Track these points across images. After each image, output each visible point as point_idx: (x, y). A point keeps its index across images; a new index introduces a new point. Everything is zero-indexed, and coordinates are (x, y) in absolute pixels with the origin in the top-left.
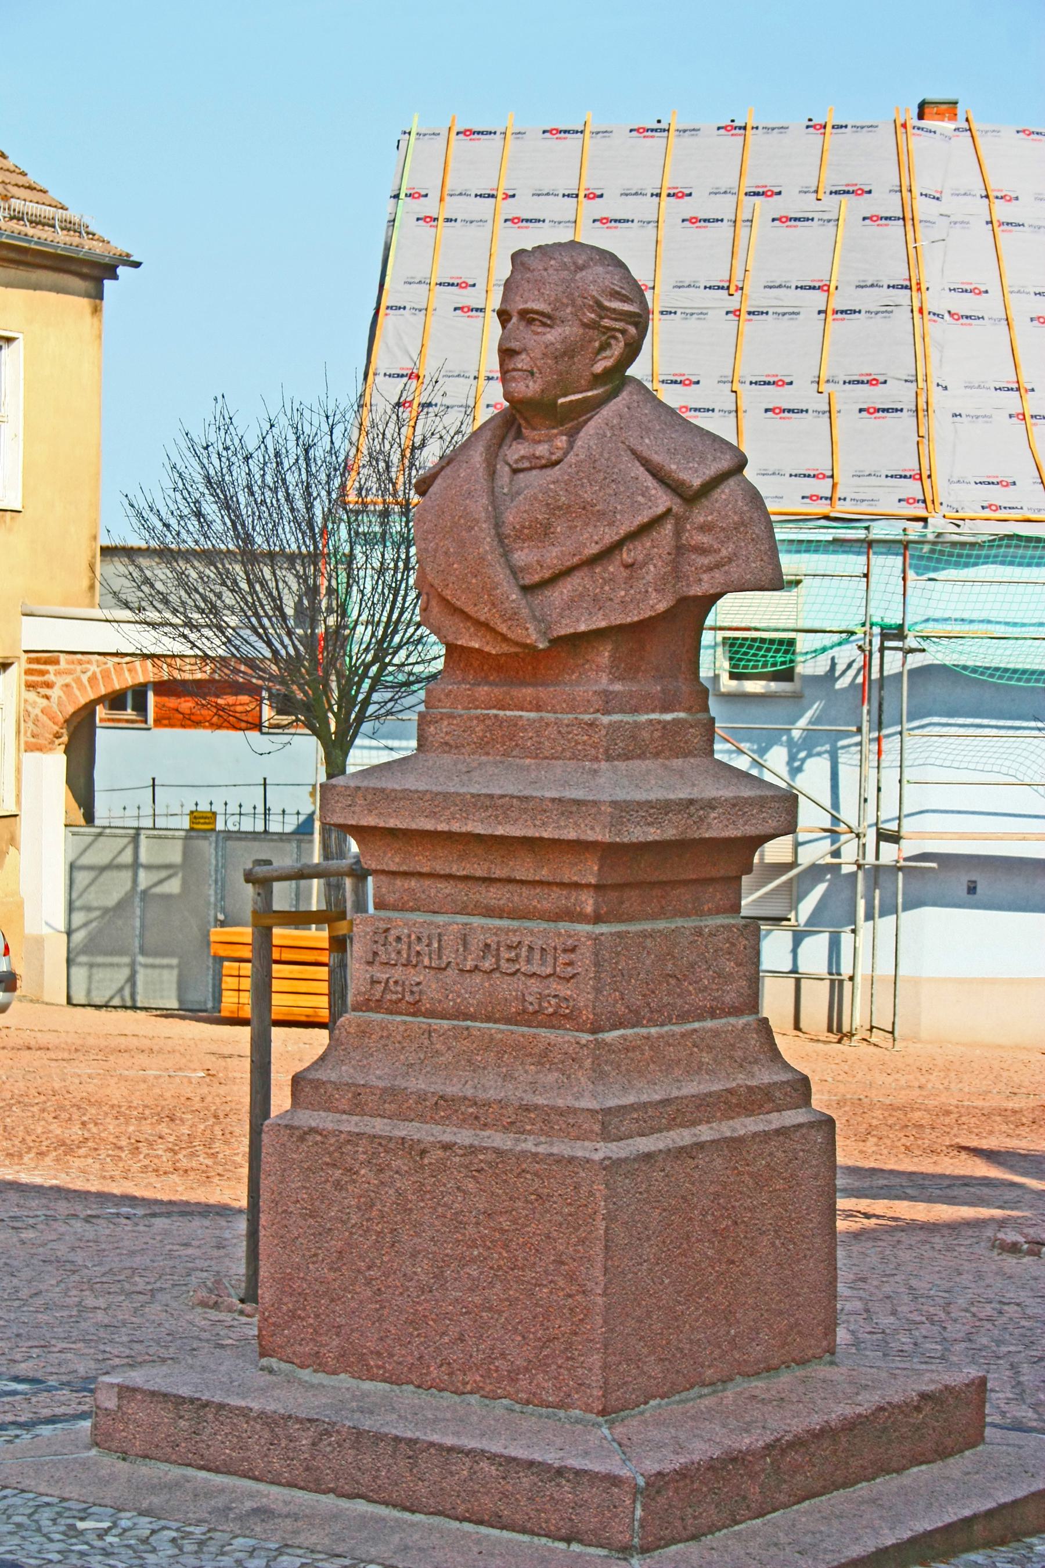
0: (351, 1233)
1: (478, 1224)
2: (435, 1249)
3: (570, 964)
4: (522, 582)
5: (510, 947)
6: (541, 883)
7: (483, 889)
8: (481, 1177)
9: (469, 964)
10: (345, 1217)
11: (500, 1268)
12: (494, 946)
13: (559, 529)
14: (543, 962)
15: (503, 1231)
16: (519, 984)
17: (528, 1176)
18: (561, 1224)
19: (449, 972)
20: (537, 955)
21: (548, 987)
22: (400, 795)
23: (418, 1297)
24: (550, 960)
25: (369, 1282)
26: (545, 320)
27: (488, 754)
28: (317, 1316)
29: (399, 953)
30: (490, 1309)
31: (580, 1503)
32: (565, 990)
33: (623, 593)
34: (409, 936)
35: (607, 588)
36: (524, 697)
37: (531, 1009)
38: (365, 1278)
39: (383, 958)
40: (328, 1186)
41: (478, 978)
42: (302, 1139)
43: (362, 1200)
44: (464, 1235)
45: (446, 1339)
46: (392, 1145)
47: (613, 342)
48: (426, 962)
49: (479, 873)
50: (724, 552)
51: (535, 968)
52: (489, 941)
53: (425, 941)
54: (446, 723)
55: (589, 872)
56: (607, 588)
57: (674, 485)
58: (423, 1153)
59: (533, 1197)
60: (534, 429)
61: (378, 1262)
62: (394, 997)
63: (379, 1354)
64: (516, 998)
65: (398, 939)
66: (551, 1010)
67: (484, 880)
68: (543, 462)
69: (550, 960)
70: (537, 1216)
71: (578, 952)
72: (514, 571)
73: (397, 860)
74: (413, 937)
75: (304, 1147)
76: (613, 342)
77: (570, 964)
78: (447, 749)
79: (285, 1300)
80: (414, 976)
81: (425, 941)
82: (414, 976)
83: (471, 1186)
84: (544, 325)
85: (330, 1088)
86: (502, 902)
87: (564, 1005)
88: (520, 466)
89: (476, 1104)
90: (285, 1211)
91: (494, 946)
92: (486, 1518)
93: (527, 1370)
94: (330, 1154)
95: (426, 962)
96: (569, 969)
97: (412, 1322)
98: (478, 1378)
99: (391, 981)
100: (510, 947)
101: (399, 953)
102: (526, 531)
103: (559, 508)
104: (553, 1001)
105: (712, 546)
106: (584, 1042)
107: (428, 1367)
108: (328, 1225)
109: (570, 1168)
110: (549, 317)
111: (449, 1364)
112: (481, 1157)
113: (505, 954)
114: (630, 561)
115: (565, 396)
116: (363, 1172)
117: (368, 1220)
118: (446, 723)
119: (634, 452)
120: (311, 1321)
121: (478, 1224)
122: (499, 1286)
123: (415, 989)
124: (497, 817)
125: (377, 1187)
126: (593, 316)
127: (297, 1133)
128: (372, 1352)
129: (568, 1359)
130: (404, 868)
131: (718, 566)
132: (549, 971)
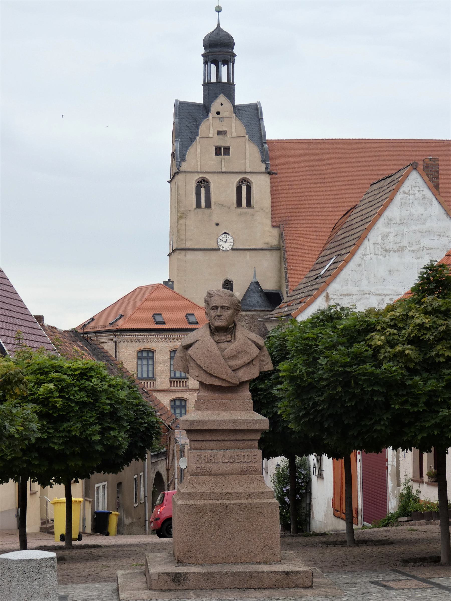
3: (255, 458)
5: (238, 456)
6: (243, 440)
7: (226, 443)
8: (244, 510)
9: (226, 461)
12: (233, 456)
14: (248, 458)
16: (241, 465)
25: (211, 540)
28: (196, 550)
29: (205, 460)
30: (248, 541)
32: (254, 465)
36: (319, 400)
39: (200, 461)
40: (198, 518)
41: (228, 464)
46: (218, 505)
48: (213, 461)
49: (226, 439)
58: (227, 506)
63: (215, 557)
69: (250, 457)
72: (230, 367)
75: (190, 509)
77: (255, 458)
81: (213, 456)
82: (209, 465)
83: (242, 512)
84: (227, 309)
85: (194, 494)
88: (219, 341)
91: (233, 456)
93: (259, 554)
94: (199, 510)
100: (238, 456)
101: (205, 460)
104: (251, 468)
119: (249, 339)
122: (250, 535)
130: (203, 439)
131: (267, 364)
132: (250, 460)
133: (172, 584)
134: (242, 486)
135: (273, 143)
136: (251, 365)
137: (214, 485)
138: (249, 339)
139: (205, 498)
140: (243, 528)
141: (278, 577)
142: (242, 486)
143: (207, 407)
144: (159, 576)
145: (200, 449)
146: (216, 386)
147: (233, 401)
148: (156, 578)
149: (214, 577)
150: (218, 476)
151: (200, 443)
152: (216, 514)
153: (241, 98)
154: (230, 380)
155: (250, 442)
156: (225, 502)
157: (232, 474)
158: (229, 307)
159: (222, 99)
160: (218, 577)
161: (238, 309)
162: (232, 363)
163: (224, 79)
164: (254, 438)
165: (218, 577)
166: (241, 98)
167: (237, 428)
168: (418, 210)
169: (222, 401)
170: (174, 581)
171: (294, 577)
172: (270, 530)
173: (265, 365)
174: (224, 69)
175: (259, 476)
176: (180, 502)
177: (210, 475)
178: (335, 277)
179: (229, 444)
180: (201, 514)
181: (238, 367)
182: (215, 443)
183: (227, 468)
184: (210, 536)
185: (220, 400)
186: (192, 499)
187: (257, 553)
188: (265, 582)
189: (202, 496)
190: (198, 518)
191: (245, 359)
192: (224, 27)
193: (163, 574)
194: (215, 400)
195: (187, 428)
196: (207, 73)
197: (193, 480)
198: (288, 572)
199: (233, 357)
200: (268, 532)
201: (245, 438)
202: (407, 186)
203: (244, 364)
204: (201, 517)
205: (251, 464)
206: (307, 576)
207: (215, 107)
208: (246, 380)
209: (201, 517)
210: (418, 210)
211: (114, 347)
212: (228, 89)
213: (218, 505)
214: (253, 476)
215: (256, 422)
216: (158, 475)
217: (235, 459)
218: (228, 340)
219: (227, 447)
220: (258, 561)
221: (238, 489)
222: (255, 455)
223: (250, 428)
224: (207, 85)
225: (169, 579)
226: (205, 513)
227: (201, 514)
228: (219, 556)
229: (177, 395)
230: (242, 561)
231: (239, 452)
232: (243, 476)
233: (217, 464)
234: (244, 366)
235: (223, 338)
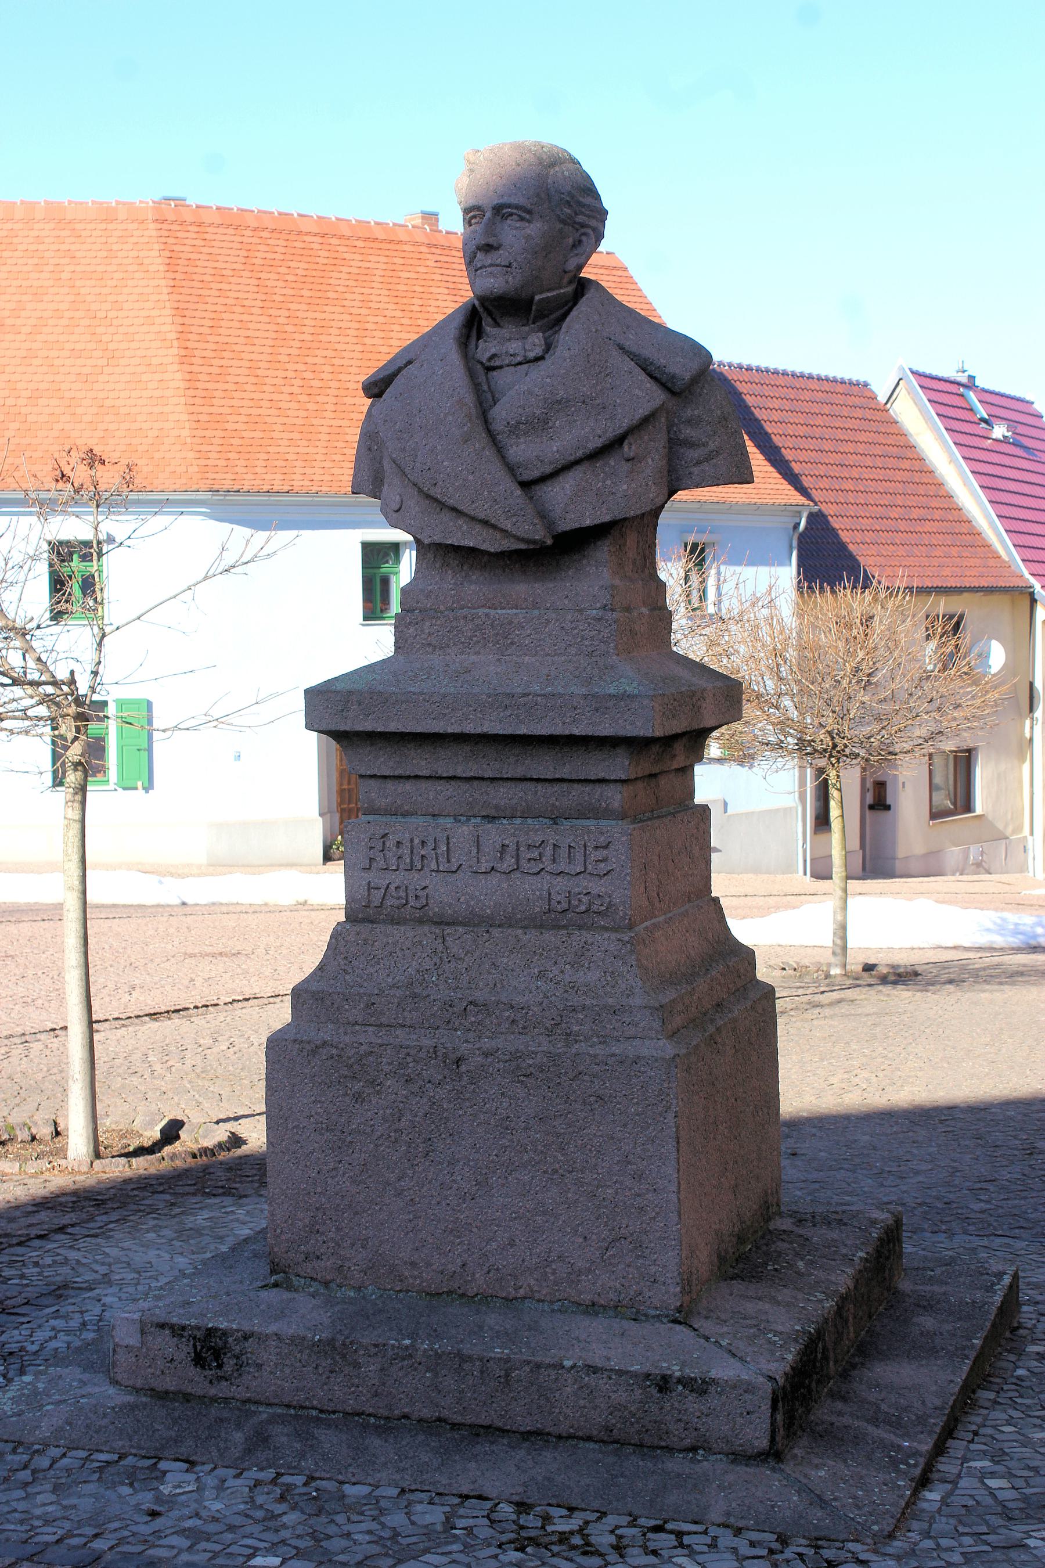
0: (377, 1146)
1: (527, 1129)
2: (477, 1156)
4: (520, 479)
10: (368, 1130)
11: (555, 1171)
12: (512, 847)
13: (558, 423)
14: (570, 858)
15: (558, 1135)
16: (544, 883)
17: (586, 1078)
18: (625, 1125)
19: (460, 874)
20: (563, 852)
21: (578, 885)
22: (403, 698)
23: (459, 1205)
24: (579, 856)
25: (399, 1194)
26: (524, 215)
27: (478, 653)
28: (338, 1229)
31: (706, 1411)
32: (597, 887)
33: (625, 487)
34: (412, 841)
35: (609, 482)
37: (559, 908)
38: (396, 1189)
41: (494, 879)
42: (314, 1052)
43: (388, 1111)
44: (512, 1141)
45: (494, 1245)
47: (584, 238)
48: (434, 866)
49: (489, 774)
50: (712, 446)
51: (562, 866)
52: (507, 842)
53: (431, 845)
54: (428, 624)
55: (619, 765)
56: (609, 482)
57: (664, 379)
58: (458, 1062)
59: (592, 1099)
60: (497, 324)
61: (410, 1172)
62: (397, 903)
64: (540, 897)
65: (399, 843)
66: (583, 908)
67: (493, 780)
68: (519, 359)
69: (579, 856)
70: (597, 1118)
71: (612, 847)
72: (511, 469)
73: (391, 764)
74: (416, 841)
76: (584, 238)
78: (430, 649)
79: (300, 1215)
80: (416, 880)
82: (416, 880)
83: (521, 1092)
84: (522, 219)
86: (514, 801)
87: (598, 902)
89: (512, 1007)
90: (297, 1127)
92: (595, 1433)
95: (434, 866)
96: (602, 865)
97: (452, 1231)
98: (533, 1282)
99: (392, 887)
102: (522, 427)
103: (559, 402)
104: (585, 899)
105: (700, 440)
106: (627, 939)
107: (474, 1274)
108: (349, 1139)
109: (635, 1067)
110: (529, 212)
111: (498, 1269)
112: (531, 1062)
113: (526, 855)
114: (632, 454)
115: (541, 292)
116: (389, 1083)
117: (396, 1131)
118: (428, 624)
119: (621, 348)
120: (331, 1235)
121: (527, 1129)
123: (420, 893)
124: (518, 716)
125: (406, 1097)
126: (569, 211)
127: (308, 1047)
128: (406, 1263)
129: (638, 1257)
130: (399, 772)
131: (708, 459)
133: (193, 1372)
134: (540, 975)
136: (612, 461)
137: (428, 964)
138: (621, 348)
139: (384, 1020)
140: (526, 1157)
141: (621, 1396)
142: (540, 975)
143: (433, 640)
144: (143, 1332)
145: (387, 812)
146: (472, 551)
147: (536, 612)
148: (134, 1341)
149: (357, 1365)
150: (448, 930)
151: (390, 785)
152: (415, 1088)
154: (508, 525)
155: (588, 788)
157: (509, 922)
158: (529, 212)
160: (371, 1367)
161: (580, 219)
164: (602, 775)
165: (371, 1367)
167: (522, 730)
169: (492, 612)
170: (199, 1360)
171: (693, 1404)
172: (638, 1177)
173: (699, 463)
175: (613, 936)
177: (421, 921)
179: (503, 795)
180: (358, 1086)
181: (548, 469)
182: (448, 790)
183: (488, 893)
184: (392, 1177)
185: (481, 611)
187: (581, 1264)
188: (568, 1411)
190: (347, 1099)
193: (162, 1326)
194: (465, 612)
195: (333, 727)
197: (352, 938)
198: (665, 1378)
200: (628, 1183)
201: (565, 772)
203: (580, 454)
204: (358, 1098)
205: (584, 883)
206: (751, 1408)
208: (588, 523)
209: (358, 1098)
213: (423, 1055)
214: (588, 936)
217: (518, 858)
218: (531, 355)
219: (497, 807)
220: (587, 1298)
222: (606, 847)
223: (577, 732)
225: (184, 1351)
226: (372, 1083)
227: (358, 1086)
228: (429, 1264)
230: (522, 1292)
231: (538, 831)
232: (548, 935)
233: (451, 878)
234: (577, 462)
235: (514, 347)
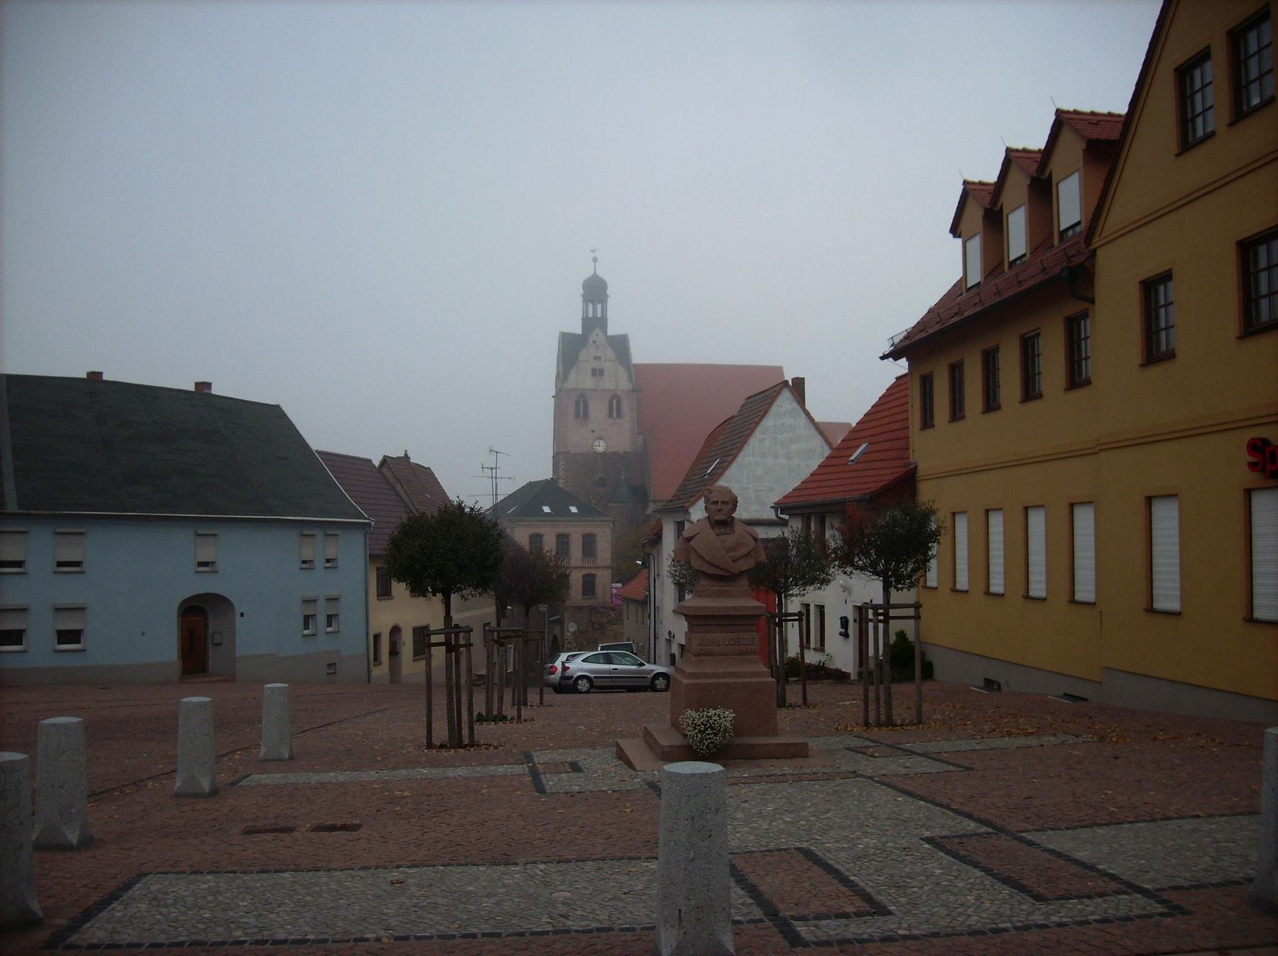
135: (637, 367)
153: (612, 331)
156: (727, 680)
159: (597, 331)
162: (731, 554)
163: (599, 315)
166: (612, 331)
168: (788, 421)
174: (599, 307)
176: (686, 681)
178: (721, 475)
186: (610, 662)
189: (706, 676)
191: (744, 550)
192: (600, 274)
196: (585, 311)
199: (734, 549)
202: (779, 401)
207: (592, 337)
210: (788, 421)
211: (1031, 557)
212: (602, 322)
215: (756, 608)
216: (555, 637)
221: (740, 669)
224: (586, 320)
229: (589, 571)
